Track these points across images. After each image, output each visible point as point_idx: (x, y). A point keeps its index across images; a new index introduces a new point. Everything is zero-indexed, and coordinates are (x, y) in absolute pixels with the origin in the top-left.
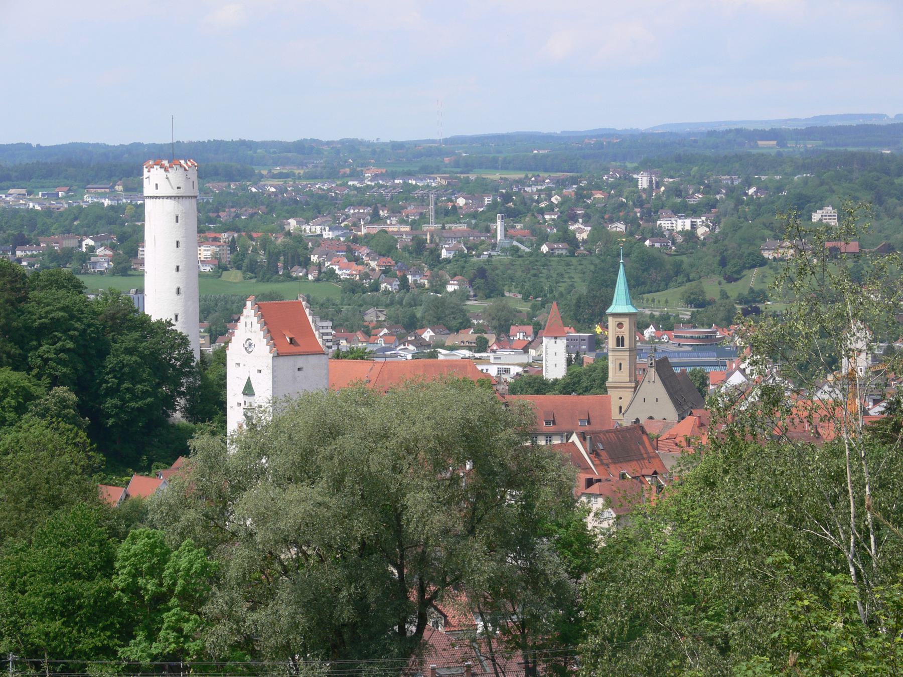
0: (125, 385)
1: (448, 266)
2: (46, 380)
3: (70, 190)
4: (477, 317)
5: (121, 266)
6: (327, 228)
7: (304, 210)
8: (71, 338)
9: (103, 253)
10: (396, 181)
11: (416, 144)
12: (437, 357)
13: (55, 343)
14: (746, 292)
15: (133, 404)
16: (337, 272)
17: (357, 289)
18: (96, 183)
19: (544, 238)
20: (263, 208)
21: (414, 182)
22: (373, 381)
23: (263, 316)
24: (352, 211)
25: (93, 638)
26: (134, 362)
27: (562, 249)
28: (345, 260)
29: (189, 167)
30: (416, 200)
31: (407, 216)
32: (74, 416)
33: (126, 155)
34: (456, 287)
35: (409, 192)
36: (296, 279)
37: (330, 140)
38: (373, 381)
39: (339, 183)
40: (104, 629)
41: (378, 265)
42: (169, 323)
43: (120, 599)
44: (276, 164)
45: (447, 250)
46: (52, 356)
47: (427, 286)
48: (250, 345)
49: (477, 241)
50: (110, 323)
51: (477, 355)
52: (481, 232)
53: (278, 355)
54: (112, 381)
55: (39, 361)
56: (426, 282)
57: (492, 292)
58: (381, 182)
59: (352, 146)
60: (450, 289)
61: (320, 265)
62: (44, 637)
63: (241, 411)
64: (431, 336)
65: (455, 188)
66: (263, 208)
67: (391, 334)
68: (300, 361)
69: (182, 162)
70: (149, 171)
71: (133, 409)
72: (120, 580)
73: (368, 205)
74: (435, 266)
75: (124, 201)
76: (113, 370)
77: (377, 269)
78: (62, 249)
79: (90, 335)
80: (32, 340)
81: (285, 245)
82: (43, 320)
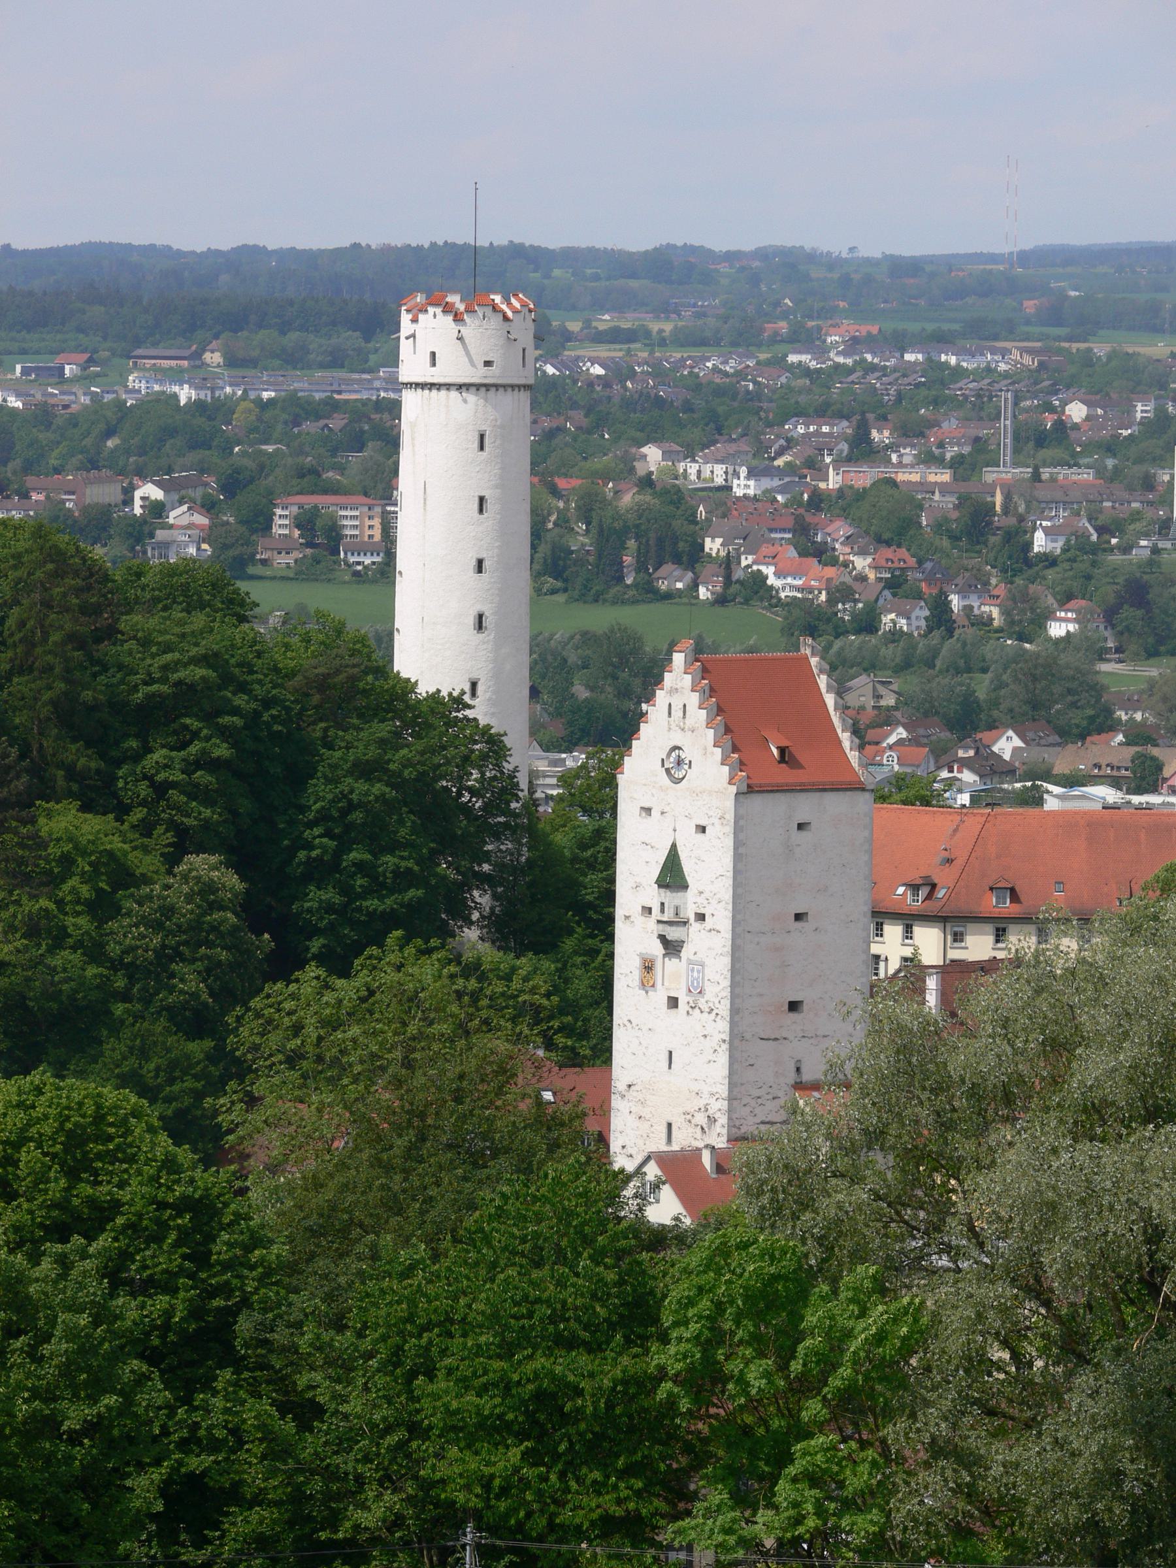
1: (1051, 574)
2: (163, 837)
3: (91, 361)
4: (1131, 704)
5: (231, 553)
6: (743, 471)
7: (681, 425)
8: (225, 733)
9: (185, 520)
10: (909, 357)
11: (950, 262)
12: (1040, 802)
13: (183, 746)
15: (372, 904)
16: (772, 581)
17: (822, 627)
18: (155, 344)
20: (578, 415)
21: (953, 360)
22: (960, 862)
23: (712, 691)
24: (801, 430)
25: (599, 1494)
26: (377, 798)
28: (792, 553)
29: (516, 311)
30: (961, 405)
31: (941, 445)
32: (235, 929)
33: (224, 278)
34: (1072, 627)
35: (943, 384)
36: (668, 596)
37: (733, 247)
38: (960, 862)
39: (763, 356)
40: (627, 1472)
41: (875, 567)
42: (458, 702)
43: (671, 1403)
44: (600, 305)
45: (1046, 531)
47: (996, 623)
48: (679, 762)
49: (1123, 512)
50: (316, 699)
51: (1136, 799)
52: (1130, 489)
53: (750, 790)
54: (321, 844)
55: (143, 789)
56: (996, 613)
57: (1161, 641)
58: (869, 357)
59: (789, 265)
60: (1057, 630)
61: (728, 564)
62: (478, 1490)
63: (651, 925)
64: (1016, 750)
65: (1054, 378)
66: (578, 415)
67: (914, 741)
68: (805, 806)
69: (498, 299)
70: (415, 320)
71: (372, 915)
72: (671, 1356)
73: (842, 416)
74: (1016, 572)
75: (228, 390)
76: (323, 817)
77: (872, 576)
78: (85, 509)
79: (268, 725)
80: (126, 736)
81: (640, 511)
82: (155, 687)
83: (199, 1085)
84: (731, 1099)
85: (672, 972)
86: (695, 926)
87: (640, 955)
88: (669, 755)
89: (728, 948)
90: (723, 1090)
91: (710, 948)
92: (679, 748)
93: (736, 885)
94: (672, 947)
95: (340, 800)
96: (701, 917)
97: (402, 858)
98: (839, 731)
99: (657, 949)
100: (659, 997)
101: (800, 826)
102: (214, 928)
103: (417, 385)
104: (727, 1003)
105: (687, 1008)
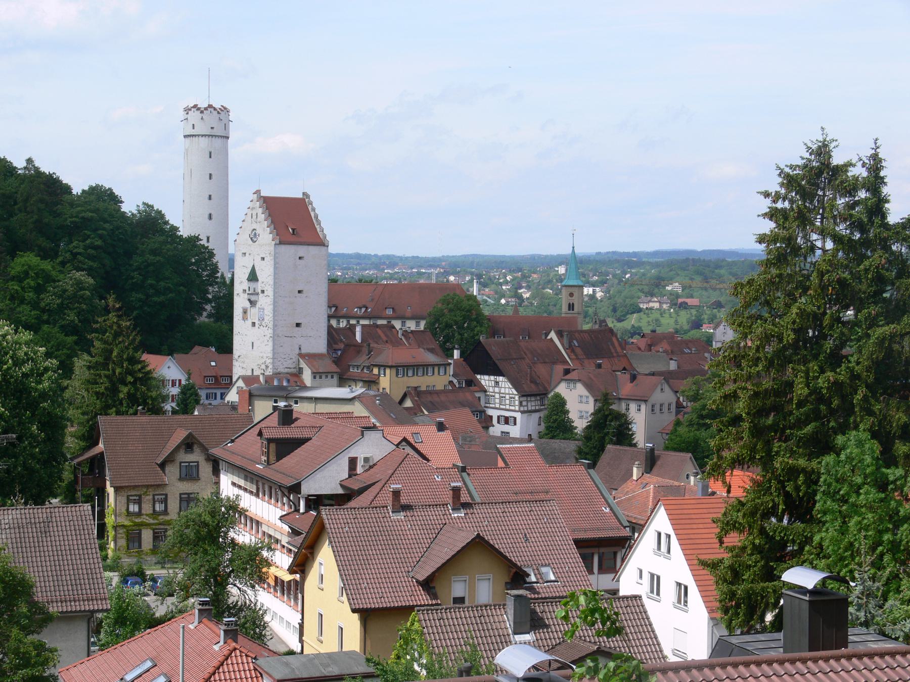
0: (149, 282)
14: (629, 327)
15: (156, 299)
19: (503, 296)
27: (513, 301)
46: (81, 250)
68: (302, 250)
83: (68, 352)
84: (273, 358)
86: (261, 295)
90: (271, 355)
91: (265, 302)
93: (275, 279)
94: (253, 303)
99: (248, 305)
100: (249, 322)
101: (300, 258)
102: (82, 297)
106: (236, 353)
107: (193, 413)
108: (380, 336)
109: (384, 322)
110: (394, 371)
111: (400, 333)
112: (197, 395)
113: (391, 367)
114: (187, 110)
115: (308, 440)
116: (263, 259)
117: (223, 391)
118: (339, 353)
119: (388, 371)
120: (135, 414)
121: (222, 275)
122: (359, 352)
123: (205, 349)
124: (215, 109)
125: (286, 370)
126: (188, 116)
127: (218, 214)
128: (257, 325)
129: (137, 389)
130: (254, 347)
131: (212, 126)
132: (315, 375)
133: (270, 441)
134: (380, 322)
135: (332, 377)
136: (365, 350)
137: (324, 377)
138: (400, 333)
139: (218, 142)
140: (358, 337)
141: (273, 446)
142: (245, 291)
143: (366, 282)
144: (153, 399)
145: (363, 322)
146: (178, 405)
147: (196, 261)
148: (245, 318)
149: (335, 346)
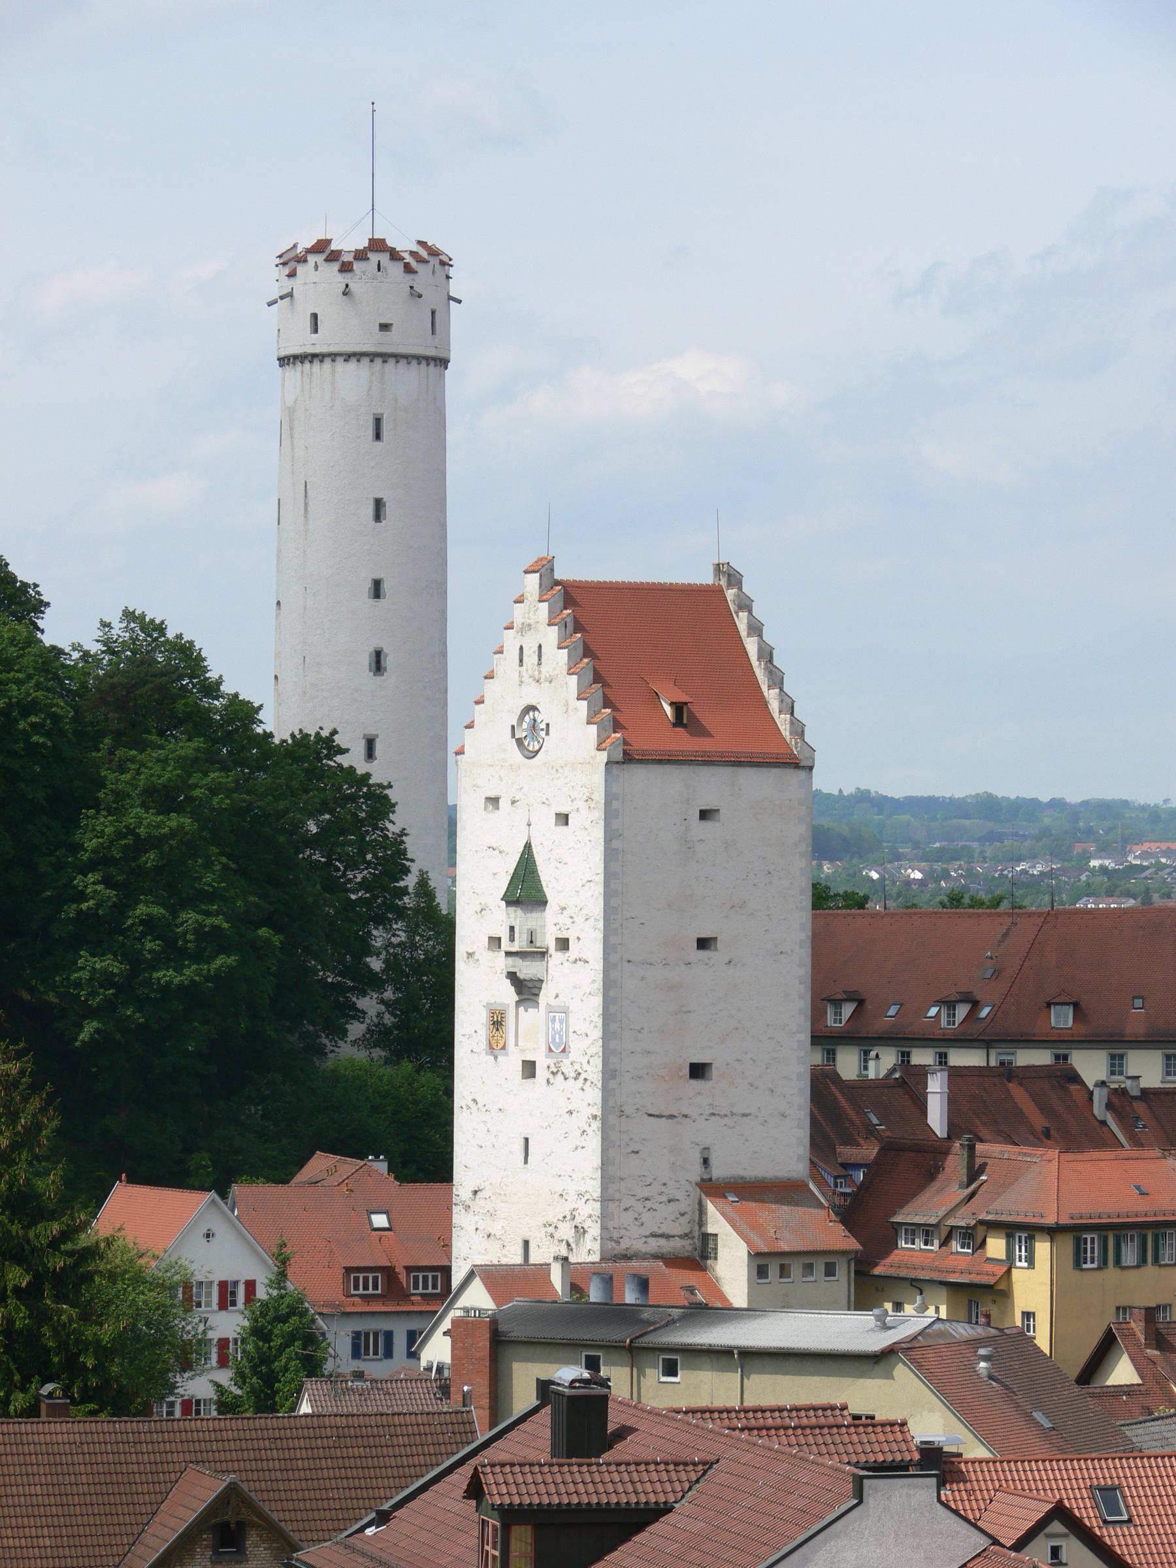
0: (141, 910)
15: (165, 975)
53: (627, 758)
68: (710, 786)
84: (606, 1199)
85: (530, 1029)
86: (556, 957)
87: (487, 1006)
88: (521, 719)
89: (599, 984)
90: (594, 1188)
91: (575, 986)
92: (533, 708)
93: (608, 894)
94: (526, 990)
95: (125, 836)
96: (563, 944)
97: (208, 914)
98: (764, 688)
99: (507, 994)
100: (512, 1063)
101: (704, 815)
103: (295, 357)
104: (598, 1062)
105: (548, 1075)
106: (455, 1181)
107: (294, 1407)
108: (1020, 1114)
109: (1042, 1058)
110: (1067, 1244)
111: (1099, 1098)
112: (311, 1339)
113: (1053, 1232)
114: (292, 261)
115: (660, 1511)
116: (563, 819)
117: (414, 1325)
118: (860, 1176)
119: (1043, 1248)
120: (32, 1411)
121: (423, 882)
122: (930, 1173)
123: (354, 1163)
124: (394, 255)
125: (654, 1245)
126: (297, 284)
127: (410, 651)
128: (540, 1070)
129: (41, 1317)
130: (529, 1165)
131: (386, 321)
132: (763, 1264)
133: (511, 1516)
134: (1026, 1058)
135: (830, 1271)
136: (955, 1163)
137: (796, 1269)
138: (1099, 1098)
139: (407, 378)
140: (936, 1118)
141: (522, 1539)
142: (495, 942)
143: (976, 903)
144: (104, 1353)
145: (961, 1058)
146: (241, 1378)
147: (324, 829)
148: (495, 1048)
149: (848, 1153)
